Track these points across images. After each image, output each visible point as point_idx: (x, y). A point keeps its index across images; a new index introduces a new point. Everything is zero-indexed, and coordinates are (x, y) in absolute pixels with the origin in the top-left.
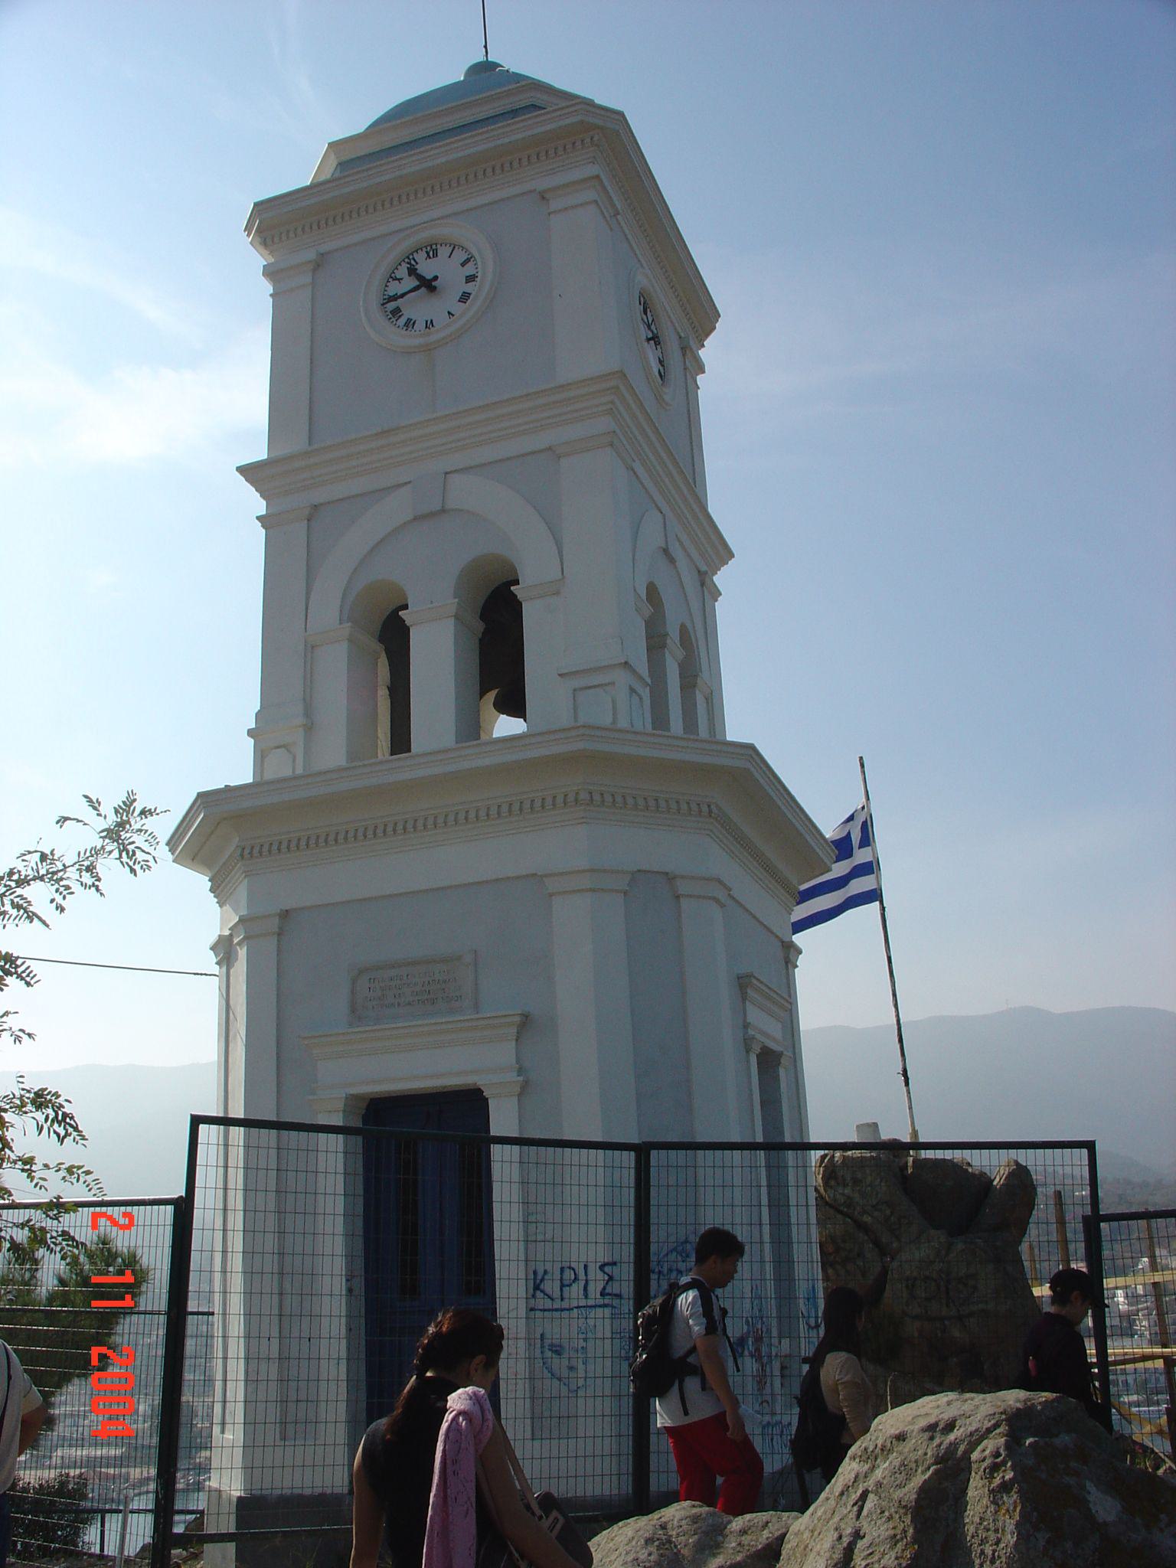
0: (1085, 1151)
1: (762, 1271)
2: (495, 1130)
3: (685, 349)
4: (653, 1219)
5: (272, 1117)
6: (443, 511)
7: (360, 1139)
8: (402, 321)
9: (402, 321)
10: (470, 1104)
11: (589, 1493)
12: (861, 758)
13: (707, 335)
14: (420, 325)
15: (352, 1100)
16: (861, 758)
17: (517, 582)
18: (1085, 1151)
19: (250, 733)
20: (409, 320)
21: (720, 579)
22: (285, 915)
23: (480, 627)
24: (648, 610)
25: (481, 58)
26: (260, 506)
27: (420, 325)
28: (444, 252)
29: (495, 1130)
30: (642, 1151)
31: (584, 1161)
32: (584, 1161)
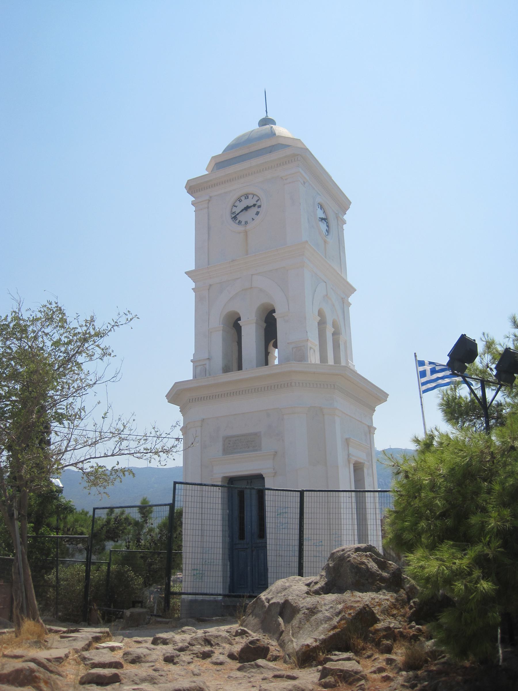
0: (177, 485)
1: (354, 533)
2: (267, 486)
3: (337, 217)
4: (305, 511)
5: (199, 482)
6: (251, 288)
7: (226, 489)
8: (237, 221)
9: (237, 221)
10: (260, 478)
11: (220, 512)
12: (415, 353)
13: (347, 210)
14: (243, 223)
15: (224, 478)
16: (415, 353)
17: (275, 312)
18: (177, 485)
19: (192, 361)
20: (240, 221)
21: (351, 299)
22: (203, 420)
23: (264, 325)
24: (319, 318)
25: (264, 116)
26: (193, 285)
27: (243, 223)
28: (250, 197)
29: (267, 486)
30: (302, 493)
31: (292, 495)
32: (294, 495)
